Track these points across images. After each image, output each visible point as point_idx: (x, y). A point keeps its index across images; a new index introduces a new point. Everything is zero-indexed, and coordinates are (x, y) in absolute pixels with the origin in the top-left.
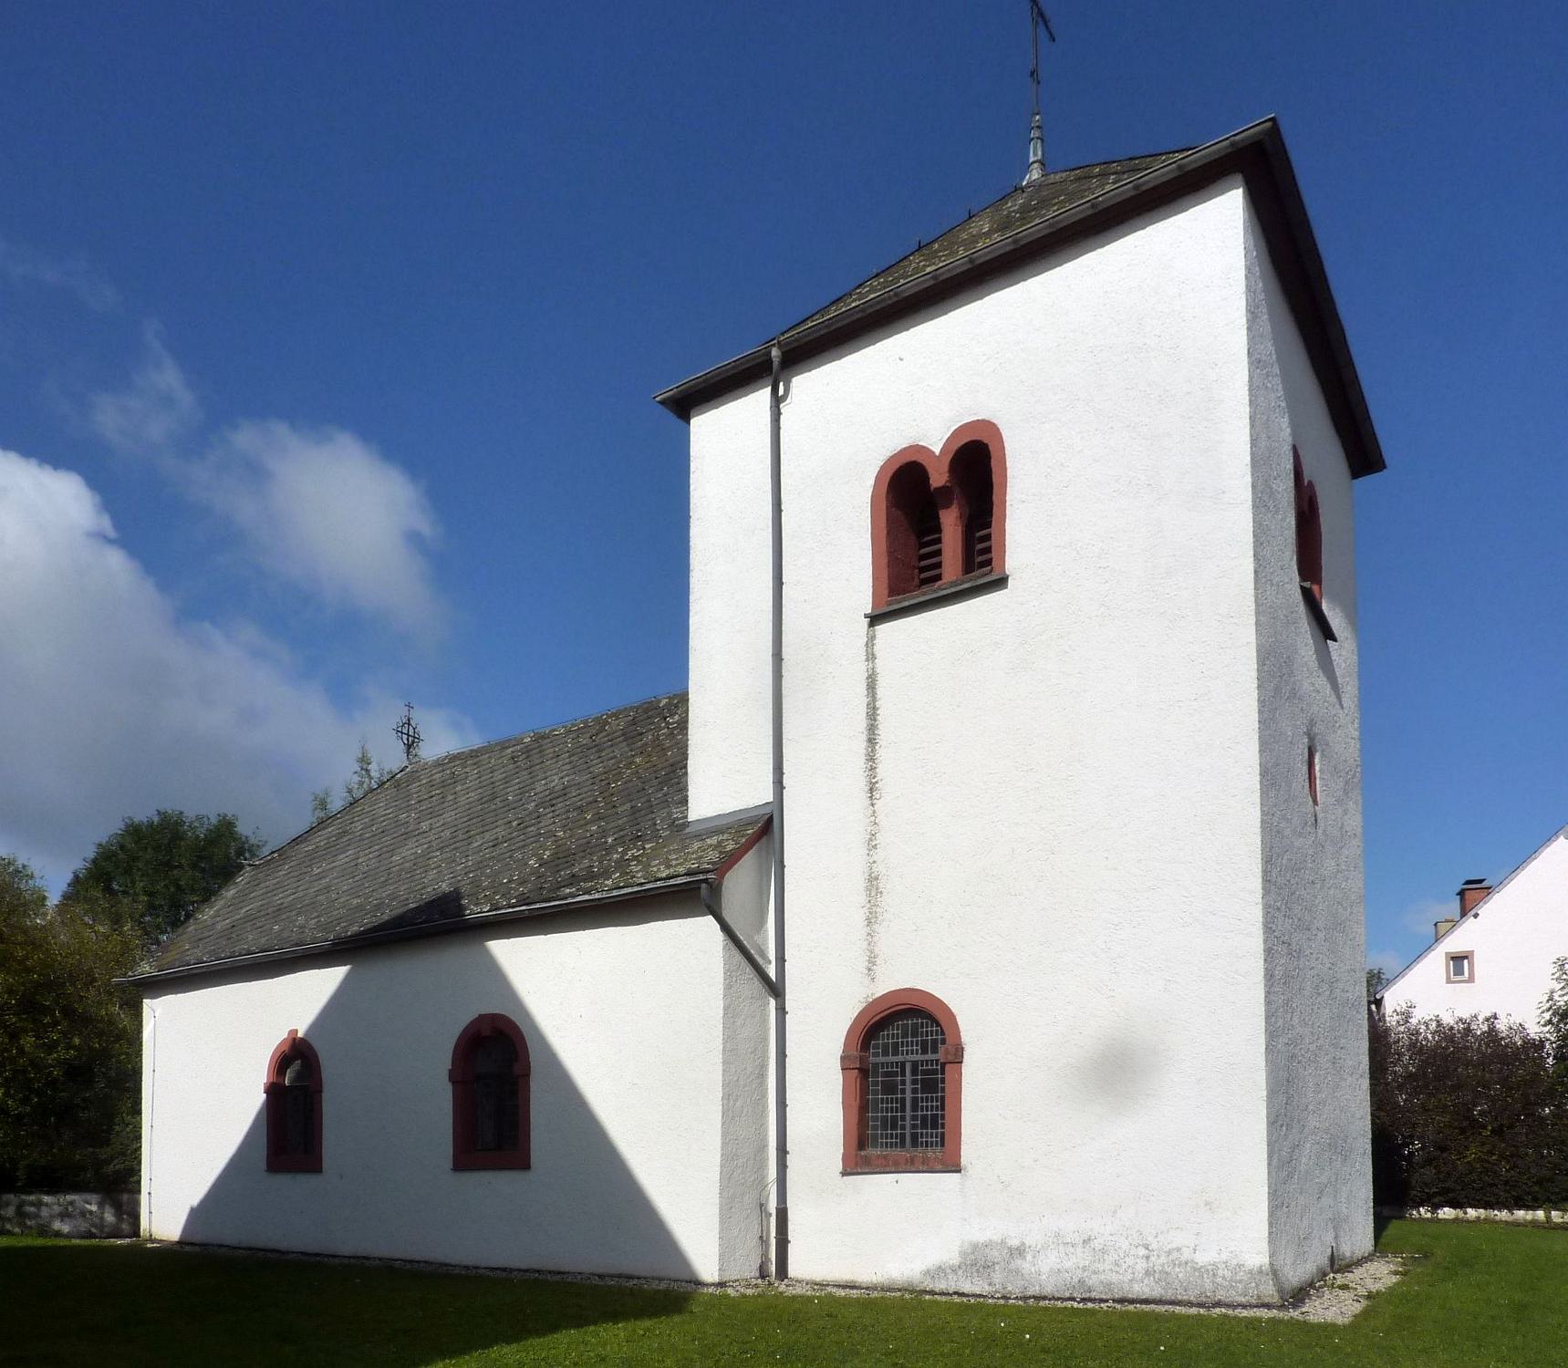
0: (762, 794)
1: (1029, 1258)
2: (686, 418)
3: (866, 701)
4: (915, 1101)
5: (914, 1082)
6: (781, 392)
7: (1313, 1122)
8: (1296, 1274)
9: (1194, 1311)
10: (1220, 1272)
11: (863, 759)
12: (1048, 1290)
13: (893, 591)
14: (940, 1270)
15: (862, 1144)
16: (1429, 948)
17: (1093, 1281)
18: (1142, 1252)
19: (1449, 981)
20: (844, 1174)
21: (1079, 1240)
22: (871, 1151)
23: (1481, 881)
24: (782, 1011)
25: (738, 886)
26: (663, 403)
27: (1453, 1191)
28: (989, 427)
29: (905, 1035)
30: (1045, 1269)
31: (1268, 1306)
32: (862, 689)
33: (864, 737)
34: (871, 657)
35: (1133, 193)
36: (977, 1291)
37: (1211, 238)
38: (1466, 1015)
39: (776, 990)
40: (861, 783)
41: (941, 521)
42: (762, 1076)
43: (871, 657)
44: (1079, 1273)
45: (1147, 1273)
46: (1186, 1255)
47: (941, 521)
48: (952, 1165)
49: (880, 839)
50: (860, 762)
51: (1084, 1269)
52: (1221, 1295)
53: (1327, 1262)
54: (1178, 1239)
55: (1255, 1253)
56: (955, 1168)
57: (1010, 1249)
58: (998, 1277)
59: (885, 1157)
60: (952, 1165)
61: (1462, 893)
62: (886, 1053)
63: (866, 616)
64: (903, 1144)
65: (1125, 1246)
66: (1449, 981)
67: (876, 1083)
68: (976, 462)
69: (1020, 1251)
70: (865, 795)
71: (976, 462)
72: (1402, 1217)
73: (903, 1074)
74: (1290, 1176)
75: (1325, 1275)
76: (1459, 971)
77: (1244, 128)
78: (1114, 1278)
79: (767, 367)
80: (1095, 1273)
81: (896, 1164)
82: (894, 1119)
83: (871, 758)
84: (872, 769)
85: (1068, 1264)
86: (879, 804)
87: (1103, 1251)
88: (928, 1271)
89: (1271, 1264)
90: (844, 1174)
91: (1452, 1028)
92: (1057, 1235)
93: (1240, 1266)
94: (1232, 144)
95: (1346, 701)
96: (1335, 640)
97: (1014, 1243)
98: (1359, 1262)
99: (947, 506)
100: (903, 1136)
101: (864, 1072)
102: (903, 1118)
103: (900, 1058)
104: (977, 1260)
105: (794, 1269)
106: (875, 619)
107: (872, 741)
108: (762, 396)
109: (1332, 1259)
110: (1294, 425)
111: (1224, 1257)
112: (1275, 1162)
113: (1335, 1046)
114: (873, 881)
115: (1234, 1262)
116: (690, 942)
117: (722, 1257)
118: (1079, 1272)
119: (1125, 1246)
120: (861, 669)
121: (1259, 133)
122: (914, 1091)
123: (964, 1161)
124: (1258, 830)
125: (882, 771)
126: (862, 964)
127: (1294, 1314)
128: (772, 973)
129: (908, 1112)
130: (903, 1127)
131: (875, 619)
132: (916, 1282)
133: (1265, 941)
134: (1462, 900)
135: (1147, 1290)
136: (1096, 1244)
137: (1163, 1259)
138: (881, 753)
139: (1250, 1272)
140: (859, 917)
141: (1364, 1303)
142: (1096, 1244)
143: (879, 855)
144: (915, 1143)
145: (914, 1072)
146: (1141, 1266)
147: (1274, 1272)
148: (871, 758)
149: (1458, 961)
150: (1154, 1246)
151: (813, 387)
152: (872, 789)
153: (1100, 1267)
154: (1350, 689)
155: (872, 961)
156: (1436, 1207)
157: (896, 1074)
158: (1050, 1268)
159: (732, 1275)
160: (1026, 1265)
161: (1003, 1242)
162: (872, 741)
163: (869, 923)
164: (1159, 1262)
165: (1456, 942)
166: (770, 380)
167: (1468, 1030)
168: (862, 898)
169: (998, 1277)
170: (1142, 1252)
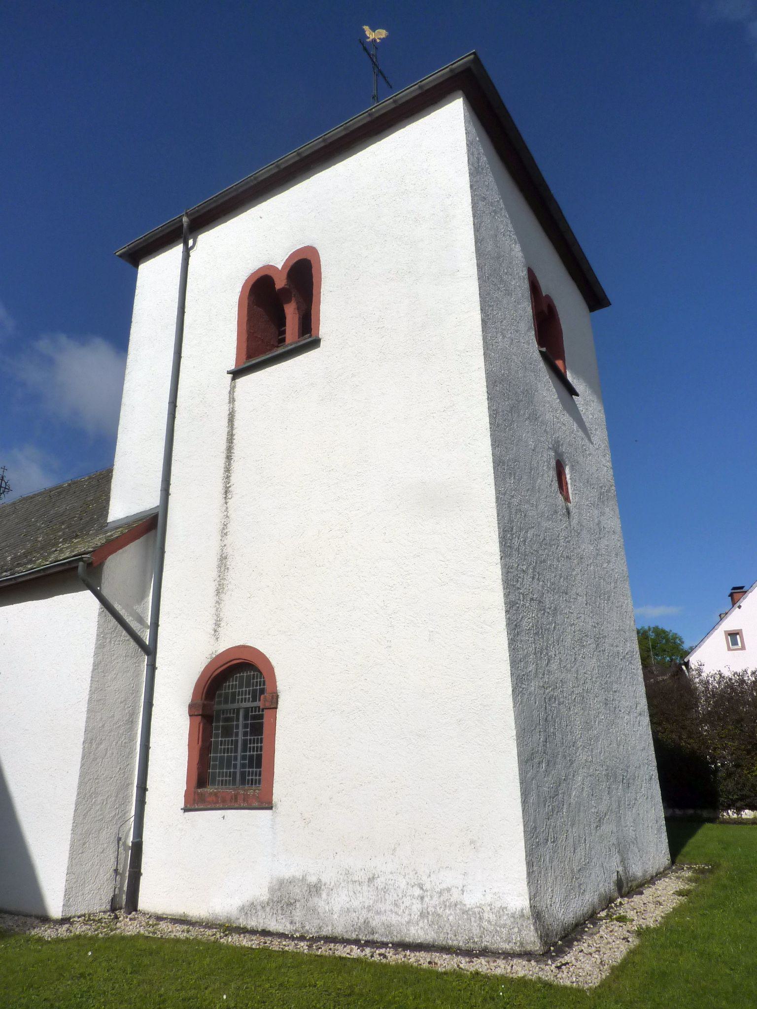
1: (324, 896)
2: (136, 265)
3: (226, 430)
4: (245, 743)
5: (245, 726)
6: (191, 242)
7: (582, 757)
8: (564, 911)
10: (486, 916)
11: (222, 470)
13: (249, 357)
16: (714, 628)
18: (417, 892)
19: (729, 649)
22: (209, 789)
23: (742, 588)
25: (121, 568)
26: (120, 256)
27: (749, 797)
28: (311, 251)
29: (241, 686)
30: (337, 909)
31: (527, 955)
32: (225, 422)
33: (224, 456)
34: (232, 400)
35: (393, 106)
36: (280, 928)
37: (448, 127)
38: (739, 670)
39: (150, 651)
40: (220, 488)
41: (280, 313)
42: (132, 722)
43: (232, 400)
45: (423, 915)
46: (455, 896)
47: (280, 313)
49: (230, 528)
50: (221, 472)
51: (369, 909)
53: (613, 887)
54: (448, 879)
55: (517, 898)
56: (266, 804)
57: (309, 886)
59: (216, 794)
60: (266, 804)
61: (731, 595)
63: (229, 373)
64: (234, 783)
65: (403, 885)
66: (729, 649)
68: (303, 273)
69: (315, 889)
71: (303, 273)
72: (712, 820)
73: (238, 720)
74: (556, 810)
75: (611, 900)
76: (735, 643)
77: (461, 61)
78: (394, 919)
79: (180, 233)
80: (378, 913)
81: (246, 798)
82: (229, 758)
83: (228, 470)
84: (228, 477)
85: (356, 904)
86: (230, 502)
87: (385, 890)
89: (532, 907)
90: (186, 810)
91: (731, 679)
92: (348, 873)
93: (503, 909)
94: (451, 70)
95: (595, 439)
96: (577, 395)
97: (312, 879)
98: (652, 880)
99: (289, 301)
102: (236, 758)
103: (235, 706)
104: (283, 897)
106: (237, 374)
107: (229, 458)
108: (177, 251)
109: (619, 884)
110: (524, 249)
111: (489, 899)
112: (532, 799)
113: (607, 690)
114: (223, 559)
115: (498, 905)
116: (77, 609)
117: (68, 893)
118: (364, 912)
119: (403, 885)
121: (466, 63)
122: (245, 734)
123: (275, 798)
124: (494, 505)
127: (547, 972)
128: (146, 638)
130: (235, 766)
131: (237, 374)
133: (506, 595)
134: (732, 599)
135: (421, 933)
136: (380, 882)
137: (436, 901)
138: (236, 466)
140: (212, 587)
141: (634, 942)
143: (229, 539)
144: (243, 781)
145: (246, 717)
146: (417, 907)
147: (537, 915)
148: (228, 470)
149: (734, 636)
150: (427, 886)
151: (213, 242)
152: (227, 491)
153: (381, 906)
154: (600, 436)
155: (218, 624)
156: (739, 810)
158: (340, 910)
159: (81, 909)
161: (304, 879)
162: (229, 458)
164: (432, 902)
165: (731, 623)
166: (182, 240)
167: (742, 681)
168: (214, 574)
169: (298, 915)
170: (417, 892)
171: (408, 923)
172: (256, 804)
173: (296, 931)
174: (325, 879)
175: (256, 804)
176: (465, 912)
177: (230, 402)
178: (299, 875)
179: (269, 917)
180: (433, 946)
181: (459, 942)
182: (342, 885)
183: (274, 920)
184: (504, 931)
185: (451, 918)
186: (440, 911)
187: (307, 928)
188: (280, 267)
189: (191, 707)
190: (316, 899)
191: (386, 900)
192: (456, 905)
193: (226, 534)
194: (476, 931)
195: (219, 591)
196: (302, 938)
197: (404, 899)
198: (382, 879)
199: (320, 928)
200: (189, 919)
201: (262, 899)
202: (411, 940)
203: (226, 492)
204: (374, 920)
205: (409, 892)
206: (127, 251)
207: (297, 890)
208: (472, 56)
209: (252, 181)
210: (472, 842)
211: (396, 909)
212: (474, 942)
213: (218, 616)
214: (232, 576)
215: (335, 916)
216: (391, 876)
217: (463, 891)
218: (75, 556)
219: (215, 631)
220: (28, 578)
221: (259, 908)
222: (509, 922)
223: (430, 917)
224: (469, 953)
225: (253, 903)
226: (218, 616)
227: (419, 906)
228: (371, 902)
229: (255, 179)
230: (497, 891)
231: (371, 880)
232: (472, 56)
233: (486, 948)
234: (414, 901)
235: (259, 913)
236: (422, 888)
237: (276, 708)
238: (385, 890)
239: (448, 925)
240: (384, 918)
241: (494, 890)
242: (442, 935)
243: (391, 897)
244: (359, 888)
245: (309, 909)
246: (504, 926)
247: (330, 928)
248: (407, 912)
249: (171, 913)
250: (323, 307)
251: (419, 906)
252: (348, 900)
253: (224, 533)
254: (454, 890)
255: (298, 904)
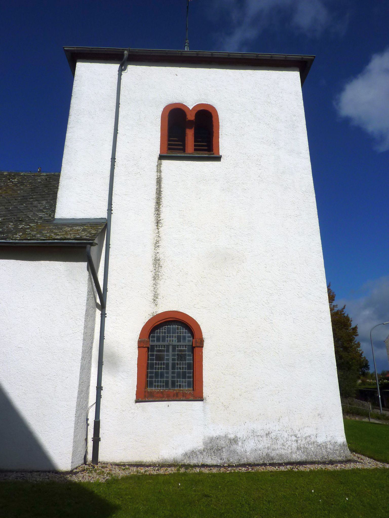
0: (104, 215)
1: (240, 444)
4: (174, 365)
6: (123, 68)
9: (320, 467)
10: (328, 446)
11: (153, 210)
12: (297, 457)
14: (193, 453)
15: (150, 384)
17: (273, 454)
20: (136, 402)
21: (263, 433)
24: (103, 316)
30: (248, 449)
33: (155, 201)
36: (214, 463)
44: (266, 451)
45: (298, 449)
46: (313, 439)
48: (198, 396)
49: (161, 243)
51: (268, 448)
52: (331, 457)
54: (308, 431)
56: (199, 397)
57: (230, 439)
58: (225, 455)
60: (198, 396)
62: (158, 340)
64: (167, 385)
65: (286, 435)
67: (152, 355)
69: (235, 441)
70: (154, 226)
73: (168, 351)
77: (307, 56)
78: (283, 452)
79: (122, 57)
80: (273, 450)
85: (260, 446)
86: (161, 229)
87: (277, 439)
88: (186, 454)
90: (136, 402)
97: (232, 436)
100: (167, 382)
101: (150, 349)
103: (166, 343)
104: (213, 446)
105: (102, 457)
111: (329, 439)
114: (157, 261)
115: (333, 441)
116: (64, 278)
119: (286, 435)
120: (154, 175)
121: (307, 59)
123: (205, 395)
125: (162, 216)
126: (150, 297)
129: (170, 370)
131: (161, 157)
132: (179, 460)
135: (299, 457)
136: (273, 435)
137: (304, 442)
139: (340, 445)
140: (149, 276)
142: (273, 435)
143: (160, 250)
146: (295, 445)
150: (299, 435)
152: (158, 222)
153: (276, 447)
157: (163, 351)
158: (251, 449)
160: (239, 448)
161: (226, 436)
162: (158, 202)
163: (155, 279)
164: (302, 443)
169: (225, 455)
170: (294, 438)
171: (291, 453)
172: (192, 398)
173: (224, 463)
174: (239, 435)
175: (192, 398)
176: (319, 446)
177: (157, 172)
178: (223, 434)
179: (206, 457)
180: (306, 462)
181: (319, 459)
182: (251, 437)
183: (210, 459)
184: (338, 452)
185: (312, 449)
186: (307, 446)
187: (231, 461)
188: (191, 108)
189: (139, 342)
190: (235, 446)
191: (277, 443)
192: (314, 443)
193: (158, 246)
194: (325, 453)
195: (156, 278)
196: (229, 466)
197: (288, 442)
198: (274, 434)
199: (239, 460)
200: (143, 464)
201: (199, 448)
202: (294, 461)
203: (157, 223)
204: (271, 453)
205: (290, 439)
206: (74, 50)
207: (223, 442)
208: (313, 58)
209: (178, 53)
210: (319, 415)
211: (284, 447)
212: (325, 458)
213: (156, 292)
214: (165, 270)
215: (248, 454)
216: (278, 432)
217: (316, 437)
218: (76, 239)
219: (154, 300)
220: (31, 245)
221: (198, 453)
222: (338, 448)
223: (302, 449)
224: (324, 463)
225: (193, 451)
226: (156, 292)
227: (296, 445)
228: (269, 445)
229: (181, 53)
230: (332, 435)
231: (267, 435)
232: (313, 58)
233: (331, 460)
234: (293, 443)
235: (199, 456)
236: (296, 437)
237: (203, 347)
238: (277, 439)
239: (311, 452)
240: (277, 452)
241: (331, 435)
242: (309, 457)
243: (280, 442)
244: (261, 439)
245: (231, 451)
246: (337, 450)
247: (245, 459)
248: (290, 448)
249: (128, 461)
250: (221, 140)
251: (296, 445)
252: (255, 445)
253: (157, 245)
254: (312, 436)
255: (224, 450)
